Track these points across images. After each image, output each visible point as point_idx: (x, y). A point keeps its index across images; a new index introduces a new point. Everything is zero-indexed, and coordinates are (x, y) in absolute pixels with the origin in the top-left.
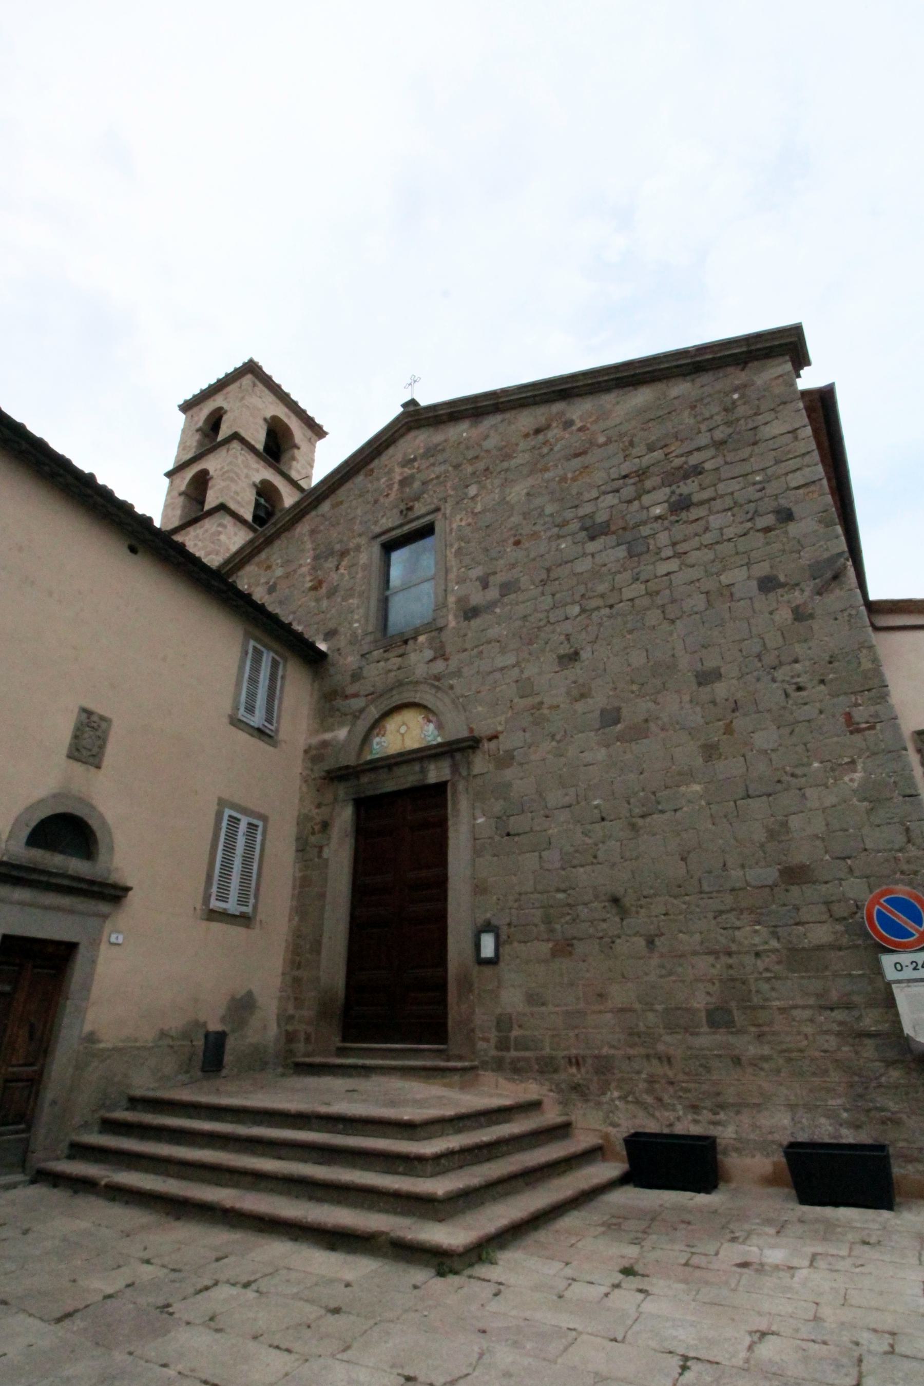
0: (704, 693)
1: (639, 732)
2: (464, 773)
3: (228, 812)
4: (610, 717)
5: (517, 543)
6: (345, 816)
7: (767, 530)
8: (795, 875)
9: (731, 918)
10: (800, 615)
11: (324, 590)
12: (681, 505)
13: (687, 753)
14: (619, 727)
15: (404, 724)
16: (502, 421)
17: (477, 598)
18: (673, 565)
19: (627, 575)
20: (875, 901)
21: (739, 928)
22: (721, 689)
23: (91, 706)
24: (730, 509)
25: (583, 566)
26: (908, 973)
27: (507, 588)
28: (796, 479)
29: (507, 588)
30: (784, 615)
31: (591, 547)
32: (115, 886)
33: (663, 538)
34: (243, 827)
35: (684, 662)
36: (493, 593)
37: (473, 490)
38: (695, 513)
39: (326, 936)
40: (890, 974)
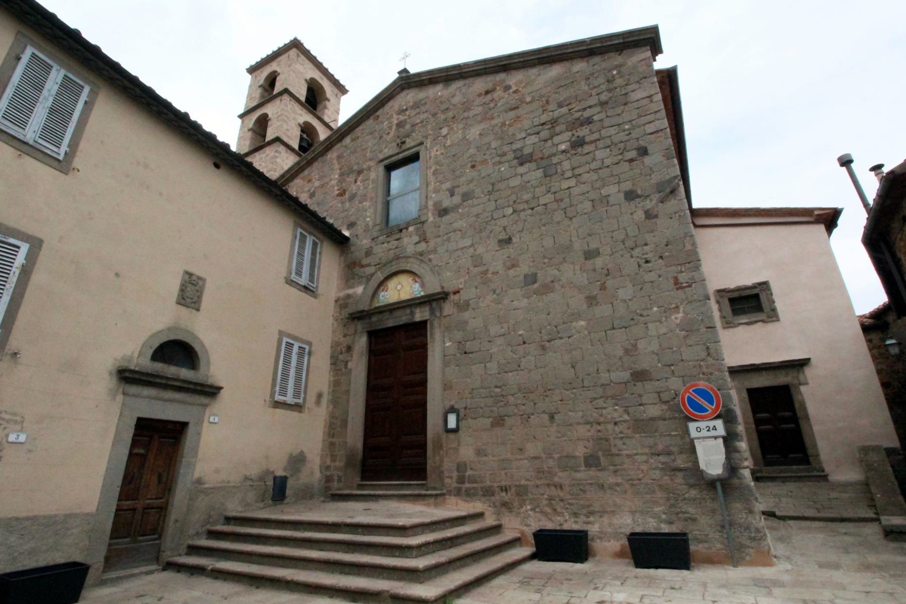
0: (589, 263)
1: (547, 288)
2: (438, 314)
4: (531, 279)
8: (640, 376)
12: (578, 143)
13: (577, 301)
17: (447, 203)
18: (572, 182)
20: (687, 390)
22: (599, 262)
26: (704, 433)
27: (466, 196)
29: (466, 196)
30: (640, 215)
31: (521, 170)
33: (566, 165)
35: (577, 245)
38: (587, 148)
40: (694, 434)
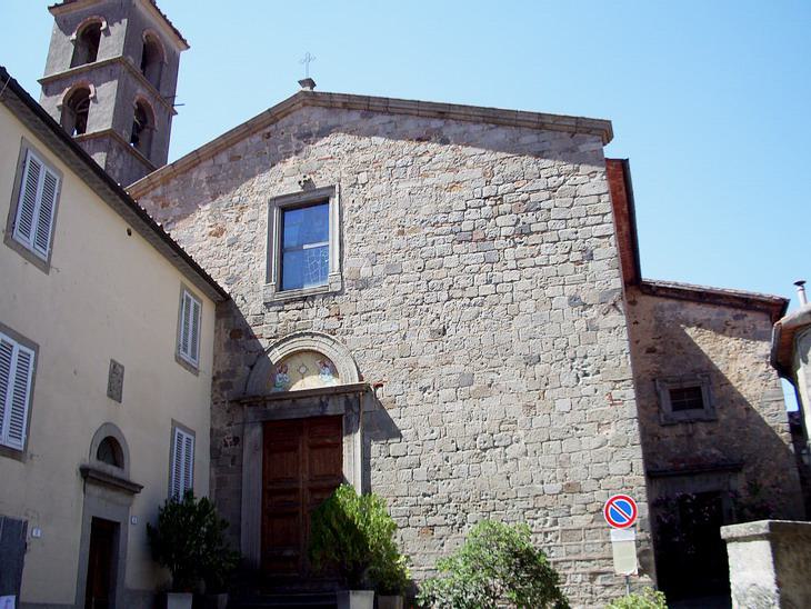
0: (530, 371)
3: (178, 430)
5: (402, 233)
6: (255, 434)
7: (578, 263)
8: (571, 488)
9: (531, 513)
10: (592, 327)
11: (225, 238)
12: (525, 232)
13: (516, 410)
14: (472, 388)
15: (303, 365)
16: (390, 122)
18: (515, 275)
19: (483, 276)
20: (610, 502)
21: (536, 519)
22: (539, 369)
23: (116, 359)
24: (555, 242)
25: (451, 261)
28: (599, 231)
29: (393, 270)
30: (581, 324)
31: (458, 248)
32: (136, 485)
33: (510, 253)
34: (184, 440)
35: (518, 347)
36: (379, 270)
37: (363, 178)
38: (535, 239)
39: (243, 523)
